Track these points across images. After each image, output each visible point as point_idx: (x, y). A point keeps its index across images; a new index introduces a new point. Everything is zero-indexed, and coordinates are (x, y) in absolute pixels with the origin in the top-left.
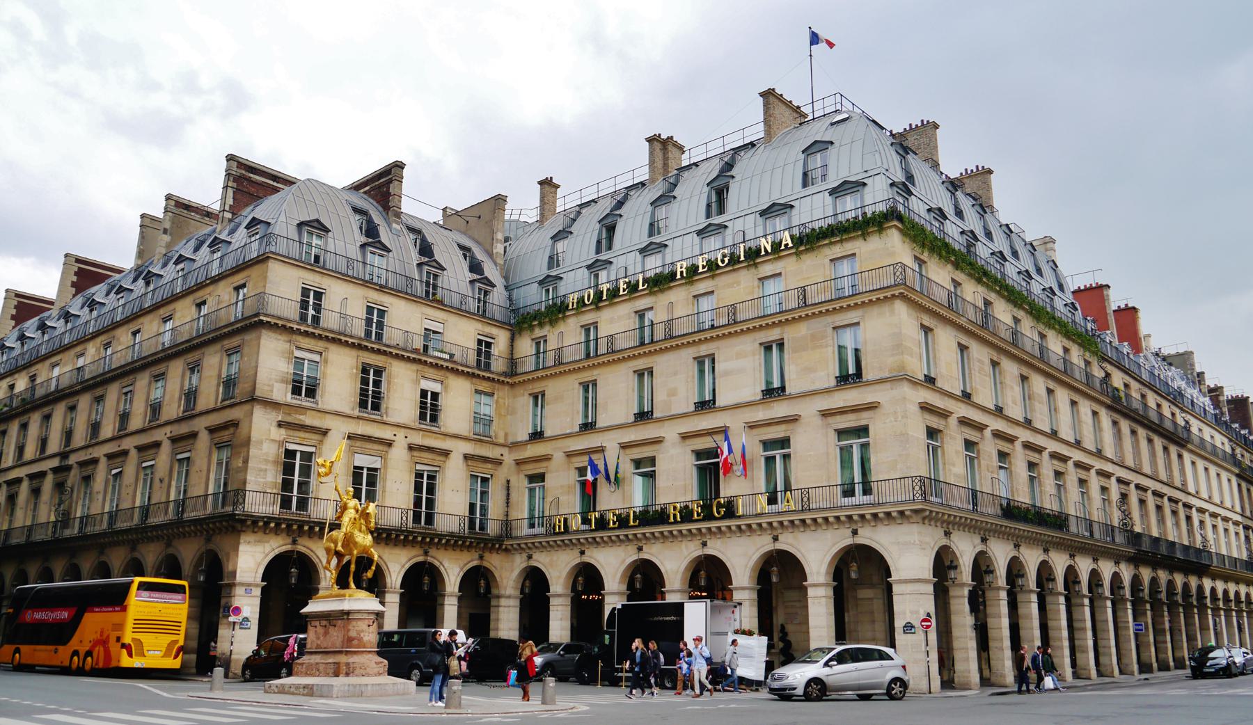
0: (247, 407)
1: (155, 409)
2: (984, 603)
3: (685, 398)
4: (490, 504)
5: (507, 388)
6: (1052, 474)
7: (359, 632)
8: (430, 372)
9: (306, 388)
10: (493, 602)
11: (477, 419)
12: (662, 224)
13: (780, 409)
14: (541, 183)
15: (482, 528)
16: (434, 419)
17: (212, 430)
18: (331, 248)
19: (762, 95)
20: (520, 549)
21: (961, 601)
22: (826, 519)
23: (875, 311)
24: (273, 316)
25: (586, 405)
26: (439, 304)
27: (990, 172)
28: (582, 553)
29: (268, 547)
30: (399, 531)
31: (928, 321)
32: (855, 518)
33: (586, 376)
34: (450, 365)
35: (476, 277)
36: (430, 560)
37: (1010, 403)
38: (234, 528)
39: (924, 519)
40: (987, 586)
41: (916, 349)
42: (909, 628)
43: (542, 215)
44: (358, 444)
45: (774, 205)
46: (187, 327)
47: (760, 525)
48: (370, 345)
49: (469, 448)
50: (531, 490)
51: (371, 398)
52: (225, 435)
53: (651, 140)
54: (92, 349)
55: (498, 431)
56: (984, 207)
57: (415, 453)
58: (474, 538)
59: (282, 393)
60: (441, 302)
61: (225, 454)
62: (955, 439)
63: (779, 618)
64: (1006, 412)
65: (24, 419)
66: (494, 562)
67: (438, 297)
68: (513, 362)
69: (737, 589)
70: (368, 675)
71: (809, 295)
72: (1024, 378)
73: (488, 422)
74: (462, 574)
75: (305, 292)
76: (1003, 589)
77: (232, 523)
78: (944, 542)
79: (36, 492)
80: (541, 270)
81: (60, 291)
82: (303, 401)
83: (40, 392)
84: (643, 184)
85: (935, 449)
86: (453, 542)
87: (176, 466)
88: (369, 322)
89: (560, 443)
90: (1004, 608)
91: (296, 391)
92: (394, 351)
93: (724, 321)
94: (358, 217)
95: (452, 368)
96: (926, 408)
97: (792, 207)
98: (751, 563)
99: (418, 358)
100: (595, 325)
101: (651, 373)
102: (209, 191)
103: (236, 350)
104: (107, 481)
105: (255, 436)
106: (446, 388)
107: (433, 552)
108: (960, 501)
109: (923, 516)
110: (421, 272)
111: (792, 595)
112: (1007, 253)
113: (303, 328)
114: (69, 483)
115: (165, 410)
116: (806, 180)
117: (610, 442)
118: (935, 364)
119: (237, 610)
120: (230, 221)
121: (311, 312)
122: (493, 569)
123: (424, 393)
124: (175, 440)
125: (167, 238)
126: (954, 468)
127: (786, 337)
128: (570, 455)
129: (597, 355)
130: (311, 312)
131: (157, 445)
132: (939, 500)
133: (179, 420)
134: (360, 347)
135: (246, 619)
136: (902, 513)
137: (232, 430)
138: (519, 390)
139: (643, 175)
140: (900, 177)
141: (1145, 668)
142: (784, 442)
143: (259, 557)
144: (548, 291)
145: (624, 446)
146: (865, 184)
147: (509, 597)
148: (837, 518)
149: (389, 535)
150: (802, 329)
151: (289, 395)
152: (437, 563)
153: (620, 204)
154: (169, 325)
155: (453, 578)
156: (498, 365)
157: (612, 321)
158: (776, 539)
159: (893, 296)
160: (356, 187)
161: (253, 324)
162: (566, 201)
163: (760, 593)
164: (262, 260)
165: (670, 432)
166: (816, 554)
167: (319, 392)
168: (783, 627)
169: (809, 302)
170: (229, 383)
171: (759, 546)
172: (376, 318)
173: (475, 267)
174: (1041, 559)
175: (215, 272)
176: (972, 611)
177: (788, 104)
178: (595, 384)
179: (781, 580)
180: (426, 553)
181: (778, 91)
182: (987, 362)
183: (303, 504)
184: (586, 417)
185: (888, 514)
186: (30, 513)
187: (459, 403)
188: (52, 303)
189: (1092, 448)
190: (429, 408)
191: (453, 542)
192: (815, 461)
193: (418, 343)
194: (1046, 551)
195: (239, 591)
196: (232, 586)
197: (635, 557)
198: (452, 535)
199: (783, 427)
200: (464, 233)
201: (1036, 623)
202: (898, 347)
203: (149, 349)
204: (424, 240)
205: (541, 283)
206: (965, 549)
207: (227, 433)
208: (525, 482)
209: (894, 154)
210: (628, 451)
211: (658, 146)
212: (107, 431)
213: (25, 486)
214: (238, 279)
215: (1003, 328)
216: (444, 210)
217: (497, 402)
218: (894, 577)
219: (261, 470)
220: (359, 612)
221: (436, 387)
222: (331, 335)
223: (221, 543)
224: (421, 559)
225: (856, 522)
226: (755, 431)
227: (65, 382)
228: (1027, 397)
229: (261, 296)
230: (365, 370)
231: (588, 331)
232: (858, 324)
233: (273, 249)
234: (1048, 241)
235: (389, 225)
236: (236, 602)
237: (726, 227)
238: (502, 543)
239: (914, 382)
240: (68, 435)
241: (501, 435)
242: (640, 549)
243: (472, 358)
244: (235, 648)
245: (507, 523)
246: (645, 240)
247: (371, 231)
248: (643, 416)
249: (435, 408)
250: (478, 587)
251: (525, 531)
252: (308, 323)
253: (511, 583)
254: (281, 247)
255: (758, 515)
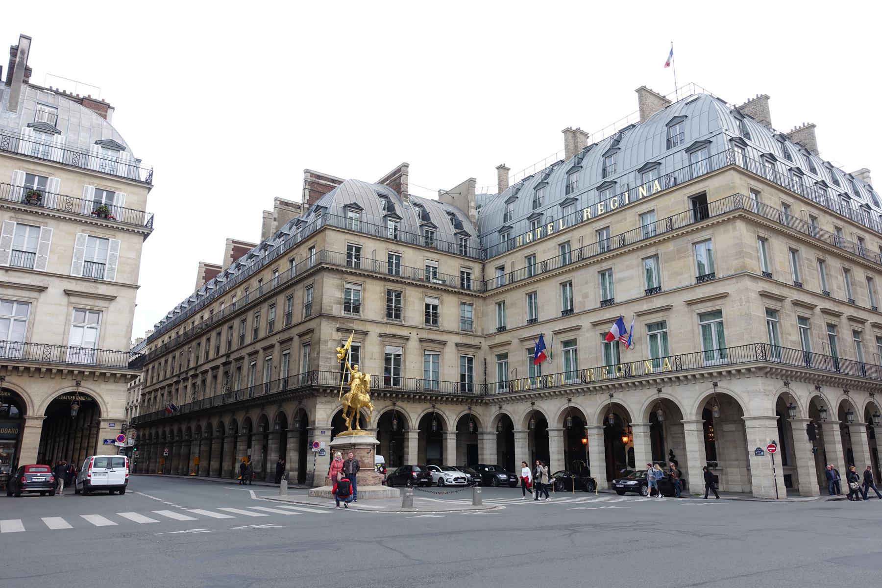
0: (318, 320)
1: (271, 324)
2: (821, 435)
3: (594, 301)
4: (474, 374)
5: (481, 300)
6: (874, 339)
7: (361, 457)
8: (431, 293)
9: (353, 306)
10: (480, 437)
11: (463, 320)
12: (575, 186)
13: (658, 302)
14: (498, 168)
15: (470, 389)
16: (435, 322)
17: (300, 336)
18: (364, 220)
19: (637, 91)
20: (494, 402)
21: (801, 432)
22: (694, 376)
23: (721, 229)
24: (330, 264)
25: (531, 307)
26: (435, 250)
27: (813, 126)
28: (533, 404)
29: (334, 406)
30: (415, 393)
31: (763, 233)
32: (715, 374)
33: (530, 289)
34: (444, 288)
35: (458, 231)
36: (436, 410)
37: (835, 288)
38: (313, 394)
39: (766, 373)
40: (875, 425)
41: (755, 254)
42: (759, 452)
43: (500, 188)
44: (387, 339)
45: (647, 164)
46: (286, 274)
47: (648, 381)
48: (391, 278)
49: (458, 339)
50: (500, 365)
51: (393, 312)
52: (307, 338)
53: (566, 131)
54: (239, 292)
55: (477, 327)
56: (809, 150)
57: (424, 344)
58: (465, 395)
59: (338, 311)
60: (436, 249)
61: (308, 349)
62: (790, 316)
63: (668, 446)
64: (832, 295)
65: (208, 335)
66: (477, 410)
67: (434, 245)
68: (484, 282)
69: (635, 425)
70: (368, 485)
71: (674, 222)
72: (846, 271)
73: (470, 323)
74: (379, 416)
75: (350, 248)
76: (836, 423)
77: (313, 391)
78: (816, 393)
79: (215, 377)
80: (499, 222)
81: (225, 261)
82: (354, 316)
83: (215, 319)
84: (562, 162)
85: (805, 330)
86: (451, 399)
87: (283, 358)
88: (390, 263)
89: (515, 333)
90: (838, 437)
91: (347, 309)
92: (407, 281)
93: (617, 245)
94: (417, 209)
95: (445, 289)
96: (764, 295)
97: (660, 164)
98: (644, 407)
99: (421, 284)
100: (534, 255)
101: (571, 285)
102: (296, 194)
103: (309, 288)
104: (249, 369)
105: (323, 337)
106: (442, 302)
107: (438, 406)
108: (796, 360)
109: (766, 372)
110: (422, 231)
111: (675, 429)
112: (829, 182)
113: (349, 270)
114: (231, 372)
115: (276, 324)
116: (669, 144)
117: (547, 331)
118: (771, 263)
119: (317, 445)
120: (308, 209)
121: (354, 260)
122: (478, 416)
123: (428, 306)
124: (282, 343)
125: (276, 223)
126: (790, 334)
127: (659, 253)
128: (522, 340)
129: (538, 274)
130: (354, 260)
131: (272, 346)
132: (778, 360)
133: (283, 331)
134: (385, 280)
135: (323, 450)
136: (749, 370)
137: (310, 335)
138: (489, 301)
139: (562, 156)
140: (737, 134)
141: (829, 484)
142: (662, 324)
143: (329, 411)
144: (504, 236)
145: (556, 333)
146: (710, 142)
147: (489, 433)
148: (702, 375)
149: (409, 396)
150: (671, 247)
151: (343, 312)
152: (441, 413)
153: (548, 175)
154: (277, 275)
155: (452, 422)
156: (475, 285)
157: (544, 252)
158: (660, 391)
159: (734, 217)
160: (382, 182)
161: (320, 269)
162: (514, 179)
163: (652, 429)
164: (323, 230)
165: (585, 322)
166: (689, 401)
167: (361, 309)
168: (671, 452)
169: (674, 227)
170: (308, 306)
171: (648, 396)
172: (394, 260)
173: (458, 225)
174: (813, 395)
175: (299, 239)
176: (810, 439)
177: (657, 96)
178: (535, 293)
179: (666, 418)
180: (434, 407)
181: (649, 87)
182: (814, 260)
183: (397, 382)
184: (531, 315)
185: (739, 371)
186: (213, 390)
187: (450, 311)
188: (221, 268)
189: (869, 307)
190: (431, 315)
191: (451, 399)
192: (684, 335)
193: (422, 275)
194: (871, 395)
195: (317, 432)
196: (313, 429)
197: (566, 406)
198: (450, 394)
199: (661, 314)
200: (452, 205)
201: (866, 448)
202: (741, 254)
203: (266, 289)
204: (424, 210)
205: (499, 231)
206: (803, 395)
207: (308, 336)
208: (496, 359)
209: (732, 119)
210: (559, 336)
211: (570, 135)
212: (248, 340)
213: (210, 374)
214: (310, 243)
215: (827, 235)
216: (439, 191)
217: (475, 309)
218: (746, 415)
219: (327, 358)
220: (361, 444)
221: (436, 302)
222: (366, 273)
223: (307, 404)
224: (431, 410)
225: (716, 377)
226: (642, 318)
227: (227, 313)
228: (851, 284)
229: (322, 252)
230: (389, 293)
231: (530, 260)
232: (710, 239)
233: (328, 223)
234: (864, 173)
235: (402, 203)
236: (316, 439)
237: (616, 182)
238: (482, 399)
239: (754, 277)
240: (230, 343)
241: (479, 330)
242: (570, 400)
243: (458, 282)
244: (317, 467)
245: (486, 386)
246: (564, 197)
247: (390, 208)
248: (568, 312)
249: (435, 315)
250: (469, 428)
251: (498, 391)
252: (352, 267)
253: (490, 424)
254: (333, 221)
255: (645, 375)
